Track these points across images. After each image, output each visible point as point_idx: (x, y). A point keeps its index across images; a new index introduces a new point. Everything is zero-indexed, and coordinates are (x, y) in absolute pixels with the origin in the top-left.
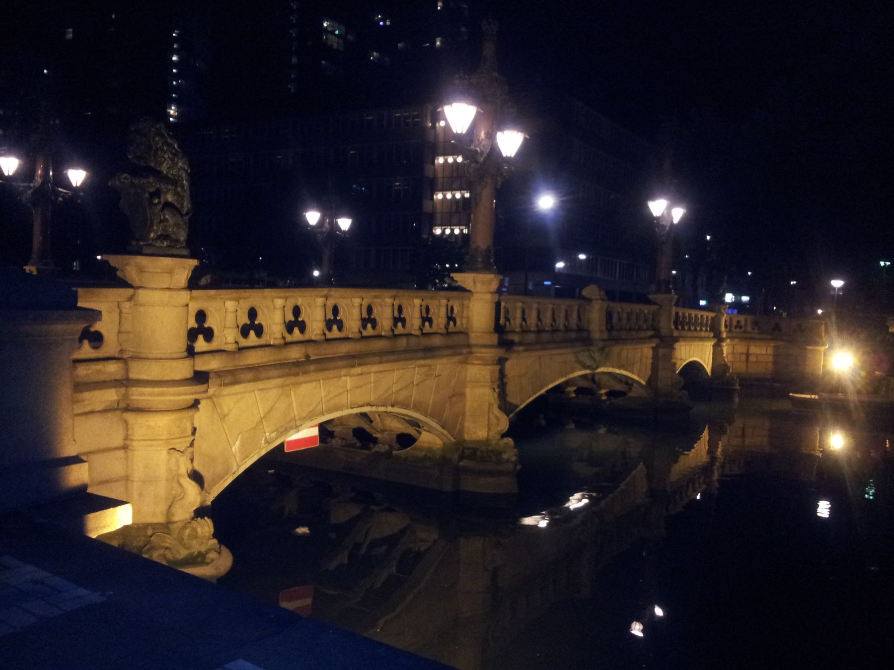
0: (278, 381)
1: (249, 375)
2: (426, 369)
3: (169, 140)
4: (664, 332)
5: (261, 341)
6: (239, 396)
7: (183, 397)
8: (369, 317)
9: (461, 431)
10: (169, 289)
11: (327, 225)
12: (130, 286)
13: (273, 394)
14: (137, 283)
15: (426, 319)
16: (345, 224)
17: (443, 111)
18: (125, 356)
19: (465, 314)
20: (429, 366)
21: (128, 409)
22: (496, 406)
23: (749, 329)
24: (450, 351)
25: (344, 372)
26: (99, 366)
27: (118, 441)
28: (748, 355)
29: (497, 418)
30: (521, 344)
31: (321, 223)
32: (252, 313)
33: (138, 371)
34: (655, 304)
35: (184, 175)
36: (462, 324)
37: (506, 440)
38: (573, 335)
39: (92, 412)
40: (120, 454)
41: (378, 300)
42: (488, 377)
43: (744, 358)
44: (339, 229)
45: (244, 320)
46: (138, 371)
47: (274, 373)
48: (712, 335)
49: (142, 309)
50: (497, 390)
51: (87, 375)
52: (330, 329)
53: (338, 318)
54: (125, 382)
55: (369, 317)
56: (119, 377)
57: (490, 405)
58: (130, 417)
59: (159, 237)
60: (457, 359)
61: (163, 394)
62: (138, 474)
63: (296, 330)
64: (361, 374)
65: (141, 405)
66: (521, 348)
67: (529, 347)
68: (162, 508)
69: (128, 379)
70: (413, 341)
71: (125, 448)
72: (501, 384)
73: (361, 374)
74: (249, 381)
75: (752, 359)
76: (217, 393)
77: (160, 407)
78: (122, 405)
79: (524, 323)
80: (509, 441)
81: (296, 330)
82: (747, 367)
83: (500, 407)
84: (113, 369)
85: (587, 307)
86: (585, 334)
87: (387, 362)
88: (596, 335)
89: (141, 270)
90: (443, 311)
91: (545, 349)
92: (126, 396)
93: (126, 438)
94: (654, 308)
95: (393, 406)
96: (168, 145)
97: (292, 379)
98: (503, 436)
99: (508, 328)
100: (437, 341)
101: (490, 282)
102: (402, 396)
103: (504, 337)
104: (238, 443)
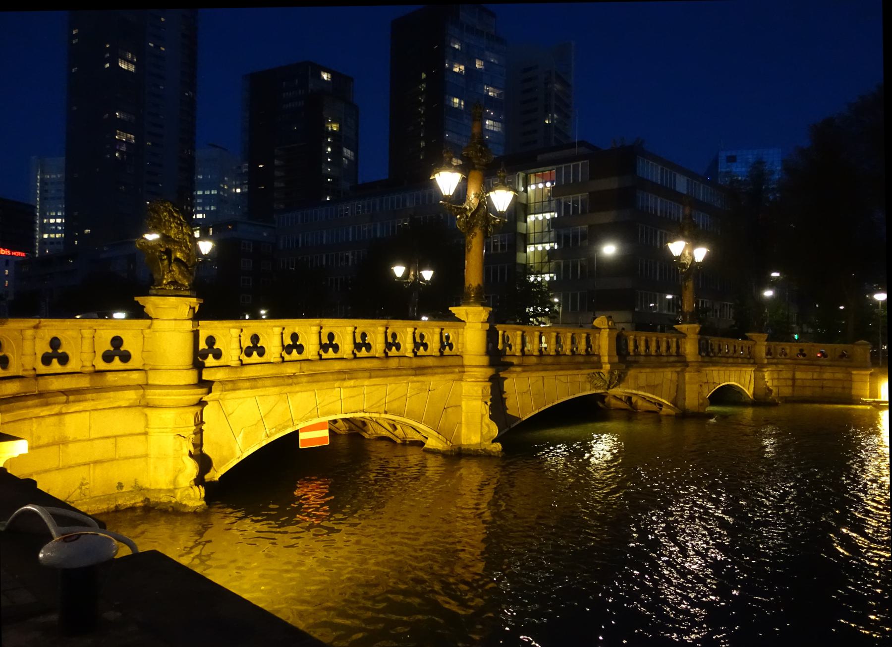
0: (276, 389)
1: (248, 384)
3: (175, 215)
5: (338, 356)
6: (241, 400)
7: (188, 397)
9: (458, 436)
10: (175, 319)
11: (412, 277)
12: (151, 318)
13: (272, 400)
14: (153, 317)
16: (427, 275)
17: (434, 179)
18: (146, 368)
21: (147, 406)
22: (487, 416)
25: (337, 384)
26: (125, 374)
27: (141, 429)
28: (794, 379)
29: (487, 425)
30: (519, 365)
31: (406, 275)
32: (255, 338)
34: (752, 340)
36: (458, 349)
37: (494, 445)
39: (120, 407)
40: (143, 438)
41: (372, 329)
42: (480, 392)
43: (790, 383)
44: (423, 280)
45: (247, 343)
47: (268, 382)
49: (157, 334)
50: (489, 403)
51: (116, 381)
54: (145, 386)
55: (394, 341)
56: (140, 383)
57: (482, 416)
58: (148, 411)
59: (169, 283)
60: (450, 376)
61: (168, 395)
62: (153, 451)
64: (354, 387)
65: (157, 403)
66: (519, 369)
67: (525, 367)
68: (170, 477)
69: (147, 385)
71: (146, 434)
73: (354, 387)
74: (248, 389)
75: (798, 383)
76: (222, 397)
77: (168, 404)
78: (143, 403)
82: (793, 391)
83: (491, 417)
84: (136, 377)
85: (597, 335)
86: (595, 358)
87: (377, 377)
89: (156, 307)
90: (437, 338)
92: (144, 396)
93: (147, 426)
94: (750, 343)
95: (386, 412)
96: (174, 217)
97: (288, 389)
100: (430, 362)
101: (480, 313)
102: (395, 405)
103: (497, 358)
104: (241, 435)
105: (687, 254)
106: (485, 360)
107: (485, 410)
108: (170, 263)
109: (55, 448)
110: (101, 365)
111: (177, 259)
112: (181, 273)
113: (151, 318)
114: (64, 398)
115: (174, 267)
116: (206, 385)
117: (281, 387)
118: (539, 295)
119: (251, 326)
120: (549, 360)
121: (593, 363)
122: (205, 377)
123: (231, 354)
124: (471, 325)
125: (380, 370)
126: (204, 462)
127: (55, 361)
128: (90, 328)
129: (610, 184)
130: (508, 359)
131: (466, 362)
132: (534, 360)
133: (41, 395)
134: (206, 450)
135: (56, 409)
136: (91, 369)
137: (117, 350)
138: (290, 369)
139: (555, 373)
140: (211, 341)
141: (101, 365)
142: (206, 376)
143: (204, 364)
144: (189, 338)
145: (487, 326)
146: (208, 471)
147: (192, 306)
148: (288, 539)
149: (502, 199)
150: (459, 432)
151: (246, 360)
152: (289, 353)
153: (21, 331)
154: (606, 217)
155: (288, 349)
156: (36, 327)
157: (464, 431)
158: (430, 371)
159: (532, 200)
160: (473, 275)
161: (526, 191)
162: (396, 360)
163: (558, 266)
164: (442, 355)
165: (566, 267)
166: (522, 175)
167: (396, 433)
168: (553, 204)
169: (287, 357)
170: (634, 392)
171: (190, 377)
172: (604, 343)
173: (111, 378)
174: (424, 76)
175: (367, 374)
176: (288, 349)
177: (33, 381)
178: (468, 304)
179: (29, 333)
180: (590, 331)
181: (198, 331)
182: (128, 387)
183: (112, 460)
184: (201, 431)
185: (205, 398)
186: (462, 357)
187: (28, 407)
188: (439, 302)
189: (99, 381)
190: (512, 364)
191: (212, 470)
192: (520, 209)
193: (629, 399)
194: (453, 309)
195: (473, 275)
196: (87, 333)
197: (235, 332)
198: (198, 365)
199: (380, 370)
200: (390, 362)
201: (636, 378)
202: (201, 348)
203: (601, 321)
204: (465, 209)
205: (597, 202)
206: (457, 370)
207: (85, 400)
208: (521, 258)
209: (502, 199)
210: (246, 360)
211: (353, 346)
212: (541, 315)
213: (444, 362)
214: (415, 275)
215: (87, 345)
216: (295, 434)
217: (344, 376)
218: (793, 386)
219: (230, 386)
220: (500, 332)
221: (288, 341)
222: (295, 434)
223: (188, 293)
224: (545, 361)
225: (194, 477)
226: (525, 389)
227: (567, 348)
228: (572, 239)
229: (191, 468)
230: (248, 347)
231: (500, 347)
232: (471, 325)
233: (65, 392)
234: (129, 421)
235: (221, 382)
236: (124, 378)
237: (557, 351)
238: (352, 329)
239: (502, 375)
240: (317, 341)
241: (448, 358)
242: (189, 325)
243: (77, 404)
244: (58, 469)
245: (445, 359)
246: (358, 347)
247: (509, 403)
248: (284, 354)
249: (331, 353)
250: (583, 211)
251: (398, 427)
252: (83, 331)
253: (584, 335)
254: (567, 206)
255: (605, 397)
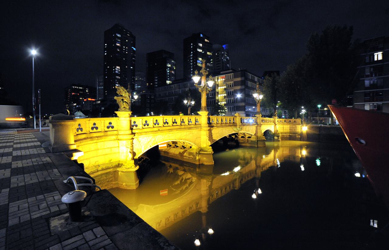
2: (189, 132)
3: (124, 90)
4: (259, 123)
5: (168, 125)
8: (157, 122)
12: (119, 117)
15: (217, 120)
19: (200, 120)
20: (191, 131)
23: (284, 122)
24: (195, 128)
29: (208, 142)
30: (216, 126)
32: (146, 122)
33: (120, 132)
35: (128, 96)
37: (210, 147)
38: (232, 124)
42: (206, 134)
43: (282, 128)
45: (144, 123)
46: (120, 132)
47: (166, 131)
48: (274, 123)
50: (208, 136)
52: (78, 131)
53: (158, 122)
54: (117, 135)
55: (157, 122)
57: (207, 140)
60: (198, 130)
63: (80, 130)
66: (216, 127)
70: (186, 126)
71: (119, 147)
72: (210, 136)
79: (217, 122)
80: (211, 147)
81: (80, 130)
84: (115, 132)
86: (235, 124)
88: (238, 124)
89: (120, 114)
90: (194, 120)
91: (93, 140)
92: (117, 137)
98: (210, 146)
99: (213, 123)
100: (192, 126)
102: (184, 138)
103: (210, 124)
105: (258, 97)
106: (207, 125)
107: (208, 138)
108: (123, 102)
109: (96, 151)
110: (106, 129)
111: (125, 102)
112: (126, 105)
113: (119, 117)
114: (97, 138)
115: (124, 103)
116: (133, 134)
117: (157, 132)
118: (221, 108)
119: (145, 118)
120: (223, 125)
121: (235, 125)
122: (133, 132)
123: (140, 126)
124: (203, 115)
125: (179, 129)
126: (134, 154)
127: (95, 129)
128: (103, 120)
129: (239, 79)
130: (213, 125)
131: (202, 126)
132: (219, 125)
133: (91, 138)
134: (134, 151)
135: (95, 141)
136: (104, 131)
137: (110, 126)
138: (155, 129)
139: (225, 128)
140: (135, 122)
141: (106, 129)
142: (134, 131)
143: (133, 128)
144: (129, 122)
145: (207, 116)
146: (135, 156)
147: (129, 113)
148: (218, 135)
149: (211, 84)
150: (200, 144)
151: (144, 127)
152: (165, 124)
153: (86, 122)
154: (238, 88)
155: (165, 123)
156: (89, 120)
157: (202, 143)
158: (192, 129)
159: (220, 83)
160: (204, 103)
161: (218, 81)
162: (184, 126)
163: (226, 100)
164: (196, 124)
165: (228, 100)
166: (217, 77)
167: (185, 144)
168: (225, 84)
169: (155, 126)
170: (245, 132)
171: (130, 132)
172: (238, 120)
173: (109, 133)
174: (192, 53)
175: (176, 130)
176: (165, 123)
177: (89, 134)
178: (202, 111)
179: (88, 122)
180: (234, 117)
181: (131, 120)
182: (113, 135)
183: (110, 154)
184: (133, 146)
185: (133, 137)
186: (201, 124)
187: (88, 141)
188: (195, 110)
189: (106, 133)
190: (214, 126)
191: (136, 156)
192: (216, 86)
193: (244, 134)
194: (198, 112)
195: (204, 103)
196: (103, 121)
197: (141, 120)
198: (132, 129)
199: (179, 129)
200: (182, 126)
201: (246, 129)
202: (132, 125)
203: (236, 114)
204: (201, 86)
205: (236, 84)
206: (199, 128)
207: (103, 139)
208: (217, 98)
209: (211, 84)
210: (144, 127)
211: (163, 123)
212: (222, 112)
213: (196, 126)
214: (190, 103)
215: (103, 125)
216: (158, 146)
217: (170, 131)
218: (283, 129)
219: (140, 134)
220: (211, 118)
221: (165, 121)
222: (158, 146)
223: (128, 110)
224: (222, 125)
225: (132, 158)
226: (218, 132)
227: (228, 122)
228: (230, 94)
229: (131, 156)
230: (155, 123)
231: (211, 122)
232: (203, 115)
233: (97, 137)
234: (115, 143)
235: (138, 133)
236: (112, 133)
237: (217, 123)
238: (172, 118)
239: (211, 129)
240: (172, 121)
241: (197, 124)
242: (129, 119)
243: (100, 140)
244: (97, 156)
245: (182, 126)
246: (174, 123)
247: (213, 136)
248: (164, 124)
249: (166, 125)
250: (232, 86)
251: (185, 143)
252: (102, 121)
253: (233, 118)
254: (228, 85)
255: (238, 133)
